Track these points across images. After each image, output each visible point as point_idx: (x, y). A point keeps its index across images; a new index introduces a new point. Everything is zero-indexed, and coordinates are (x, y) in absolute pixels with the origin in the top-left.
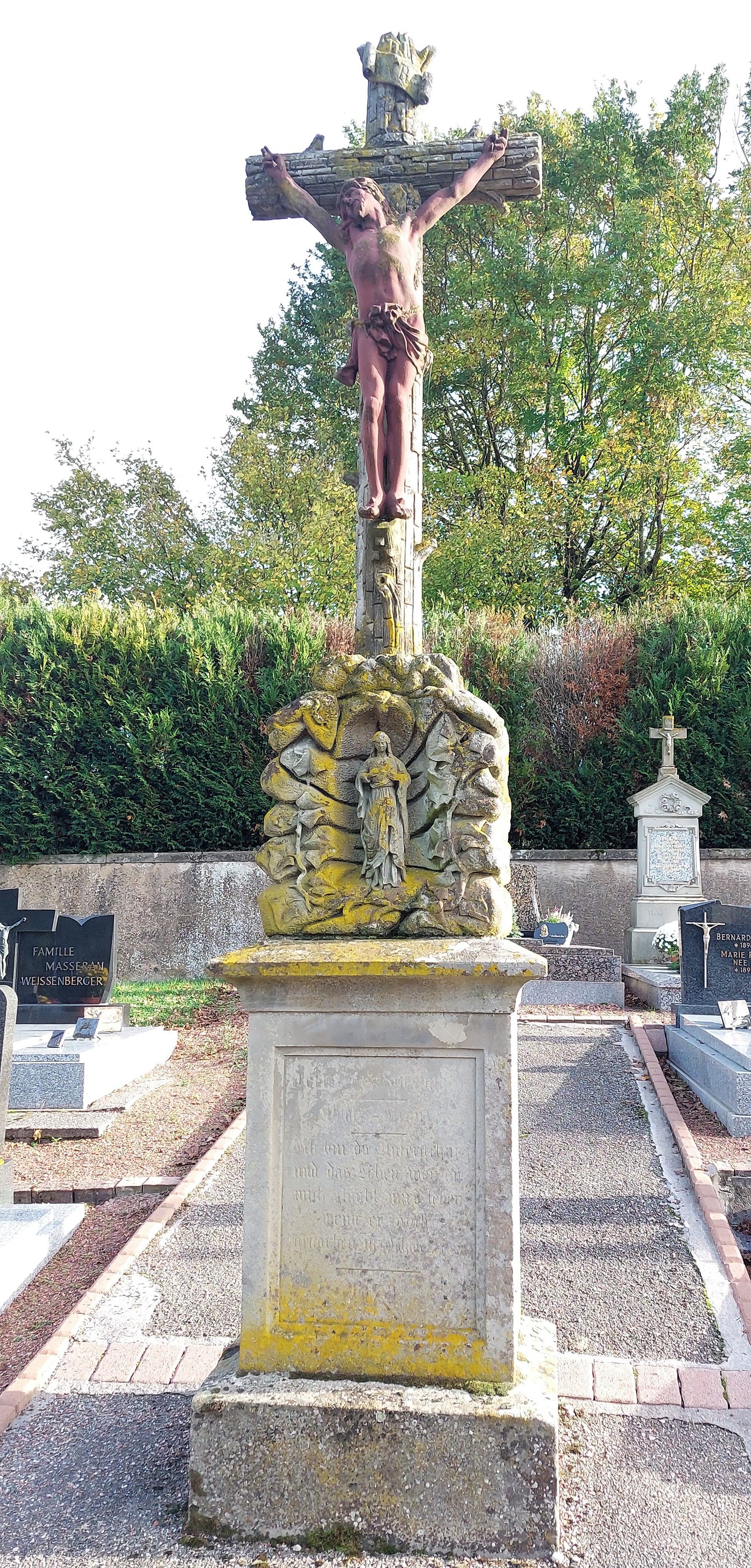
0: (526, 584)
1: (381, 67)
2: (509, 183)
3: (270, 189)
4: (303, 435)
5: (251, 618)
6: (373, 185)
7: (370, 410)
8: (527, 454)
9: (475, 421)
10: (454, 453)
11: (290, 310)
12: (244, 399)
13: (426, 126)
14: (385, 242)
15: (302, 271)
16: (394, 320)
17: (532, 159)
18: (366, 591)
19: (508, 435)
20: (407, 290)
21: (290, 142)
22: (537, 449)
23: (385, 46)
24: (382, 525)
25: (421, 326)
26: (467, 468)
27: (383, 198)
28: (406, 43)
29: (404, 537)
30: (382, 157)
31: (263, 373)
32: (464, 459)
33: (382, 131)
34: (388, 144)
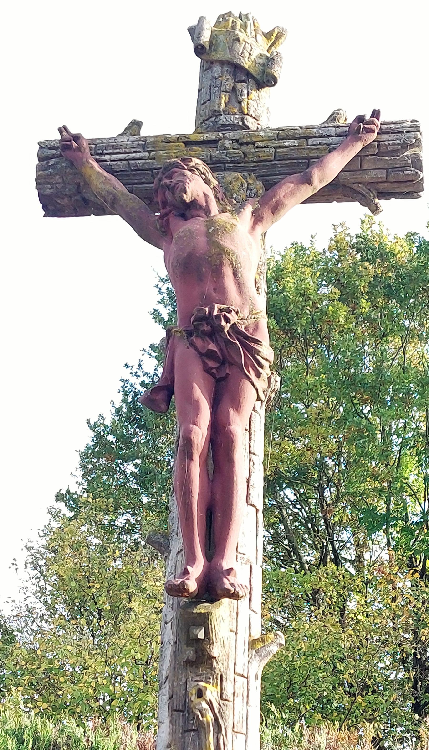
0: (371, 698)
1: (217, 45)
2: (382, 174)
3: (69, 179)
4: (128, 529)
5: (50, 730)
6: (202, 166)
7: (188, 443)
8: (367, 556)
9: (310, 519)
10: (289, 552)
11: (121, 407)
12: (68, 492)
13: (270, 112)
14: (216, 231)
15: (135, 370)
16: (227, 327)
17: (412, 146)
18: (174, 710)
19: (345, 535)
20: (246, 290)
21: (99, 125)
22: (378, 550)
23: (223, 24)
24: (202, 608)
25: (263, 336)
26: (302, 567)
27: (215, 182)
28: (250, 23)
29: (236, 628)
30: (216, 142)
31: (90, 466)
32: (300, 558)
33: (216, 114)
34: (224, 127)
